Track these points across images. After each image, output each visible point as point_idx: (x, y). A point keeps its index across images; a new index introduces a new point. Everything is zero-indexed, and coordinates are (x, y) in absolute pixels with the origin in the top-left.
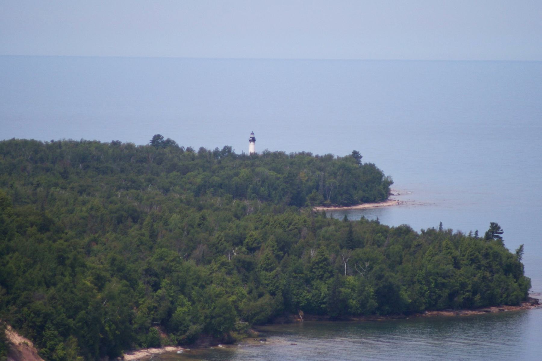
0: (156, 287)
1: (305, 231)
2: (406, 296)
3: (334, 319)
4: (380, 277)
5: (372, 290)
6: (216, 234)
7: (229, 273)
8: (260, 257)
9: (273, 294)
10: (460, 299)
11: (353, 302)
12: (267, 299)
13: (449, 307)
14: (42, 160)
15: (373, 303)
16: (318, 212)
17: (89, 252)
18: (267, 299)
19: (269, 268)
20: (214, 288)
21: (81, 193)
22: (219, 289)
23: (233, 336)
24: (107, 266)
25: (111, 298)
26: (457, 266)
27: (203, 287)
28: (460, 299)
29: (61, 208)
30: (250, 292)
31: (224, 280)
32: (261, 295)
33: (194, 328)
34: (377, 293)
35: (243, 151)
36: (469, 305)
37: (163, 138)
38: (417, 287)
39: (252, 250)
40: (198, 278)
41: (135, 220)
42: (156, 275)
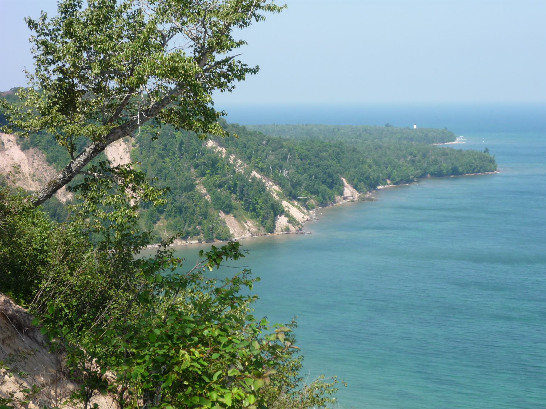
0: (387, 167)
1: (430, 151)
2: (461, 170)
3: (439, 176)
4: (453, 164)
5: (450, 168)
6: (404, 152)
7: (408, 163)
8: (417, 158)
9: (421, 169)
10: (476, 170)
11: (445, 171)
12: (419, 171)
13: (473, 172)
14: (354, 131)
15: (451, 171)
16: (434, 145)
17: (367, 158)
18: (419, 171)
19: (419, 161)
20: (404, 168)
21: (365, 140)
22: (405, 168)
23: (124, 145)
24: (372, 162)
25: (374, 171)
26: (475, 160)
27: (400, 167)
28: (476, 170)
29: (77, 76)
30: (414, 169)
31: (407, 165)
32: (417, 170)
33: (398, 179)
34: (452, 169)
35: (254, 71)
36: (479, 172)
37: (191, 57)
38: (464, 167)
39: (415, 156)
40: (399, 165)
41: (380, 148)
42: (387, 164)
